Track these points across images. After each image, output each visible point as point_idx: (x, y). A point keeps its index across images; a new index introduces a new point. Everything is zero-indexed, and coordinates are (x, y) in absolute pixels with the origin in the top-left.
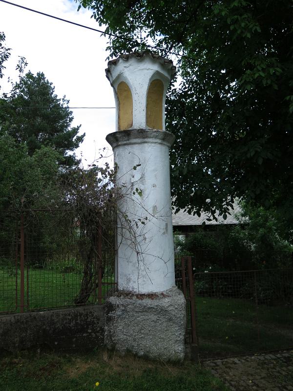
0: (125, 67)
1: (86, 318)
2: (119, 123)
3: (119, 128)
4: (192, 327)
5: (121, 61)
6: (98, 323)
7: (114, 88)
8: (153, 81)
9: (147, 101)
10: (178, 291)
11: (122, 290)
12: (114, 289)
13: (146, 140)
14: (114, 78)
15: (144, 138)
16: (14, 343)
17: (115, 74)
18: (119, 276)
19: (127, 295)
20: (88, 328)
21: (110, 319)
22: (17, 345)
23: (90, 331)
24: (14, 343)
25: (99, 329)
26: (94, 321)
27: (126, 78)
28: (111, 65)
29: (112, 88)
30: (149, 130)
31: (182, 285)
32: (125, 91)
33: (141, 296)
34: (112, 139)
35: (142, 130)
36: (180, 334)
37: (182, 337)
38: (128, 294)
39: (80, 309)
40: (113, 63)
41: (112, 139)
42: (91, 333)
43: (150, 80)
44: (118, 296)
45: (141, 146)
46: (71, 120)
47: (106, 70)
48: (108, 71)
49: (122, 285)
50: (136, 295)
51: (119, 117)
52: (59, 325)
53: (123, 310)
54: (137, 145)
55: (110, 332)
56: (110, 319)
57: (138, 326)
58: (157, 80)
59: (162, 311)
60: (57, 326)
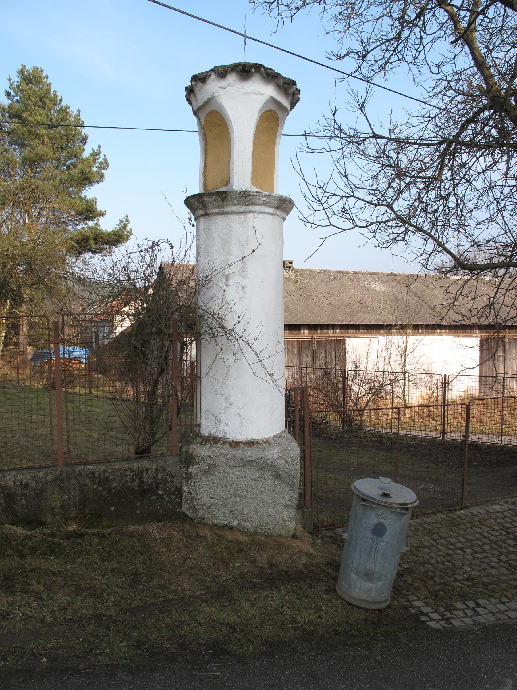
0: (220, 87)
1: (155, 474)
2: (205, 176)
3: (205, 185)
4: (305, 486)
5: (213, 76)
6: (172, 481)
7: (199, 119)
8: (264, 112)
9: (254, 144)
10: (290, 437)
11: (207, 435)
12: (192, 433)
13: (251, 208)
14: (201, 103)
15: (248, 205)
16: (53, 509)
17: (202, 97)
18: (203, 414)
19: (216, 443)
20: (158, 488)
21: (189, 477)
22: (56, 511)
23: (160, 492)
24: (53, 509)
25: (173, 489)
26: (166, 478)
27: (221, 106)
28: (196, 81)
29: (195, 119)
30: (257, 192)
31: (293, 427)
32: (219, 125)
33: (235, 444)
34: (194, 203)
35: (245, 192)
36: (292, 496)
37: (294, 501)
38: (215, 440)
39: (146, 463)
40: (200, 79)
41: (194, 203)
42: (162, 495)
43: (260, 111)
44: (201, 444)
45: (242, 217)
46: (84, 140)
47: (186, 88)
48: (190, 91)
49: (207, 428)
50: (229, 443)
51: (205, 166)
52: (116, 485)
53: (210, 464)
54: (236, 216)
55: (191, 493)
56: (189, 477)
57: (231, 486)
58: (270, 111)
59: (264, 465)
60: (113, 486)
